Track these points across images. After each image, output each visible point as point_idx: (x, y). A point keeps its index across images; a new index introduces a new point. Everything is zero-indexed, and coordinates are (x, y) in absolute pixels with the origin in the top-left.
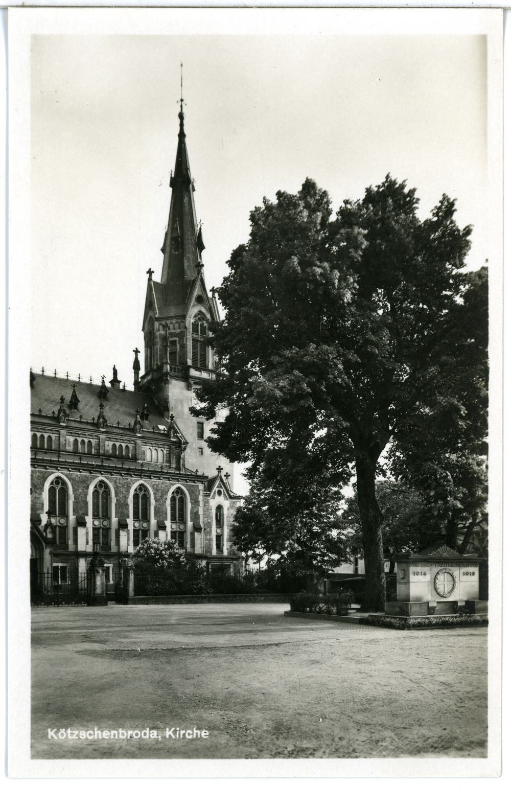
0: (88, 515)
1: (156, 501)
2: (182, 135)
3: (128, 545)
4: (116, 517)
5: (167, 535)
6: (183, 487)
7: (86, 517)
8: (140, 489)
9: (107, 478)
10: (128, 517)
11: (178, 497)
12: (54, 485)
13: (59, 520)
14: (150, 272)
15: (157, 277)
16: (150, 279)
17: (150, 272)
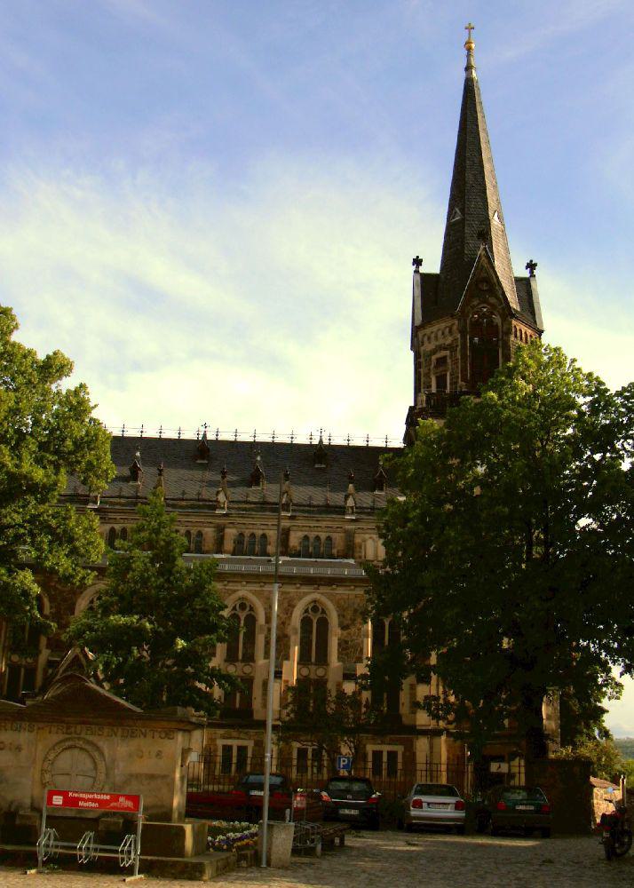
1: (344, 627)
2: (468, 68)
6: (323, 599)
8: (315, 609)
9: (255, 593)
11: (243, 615)
12: (311, 614)
14: (417, 262)
15: (433, 266)
16: (416, 272)
17: (417, 262)
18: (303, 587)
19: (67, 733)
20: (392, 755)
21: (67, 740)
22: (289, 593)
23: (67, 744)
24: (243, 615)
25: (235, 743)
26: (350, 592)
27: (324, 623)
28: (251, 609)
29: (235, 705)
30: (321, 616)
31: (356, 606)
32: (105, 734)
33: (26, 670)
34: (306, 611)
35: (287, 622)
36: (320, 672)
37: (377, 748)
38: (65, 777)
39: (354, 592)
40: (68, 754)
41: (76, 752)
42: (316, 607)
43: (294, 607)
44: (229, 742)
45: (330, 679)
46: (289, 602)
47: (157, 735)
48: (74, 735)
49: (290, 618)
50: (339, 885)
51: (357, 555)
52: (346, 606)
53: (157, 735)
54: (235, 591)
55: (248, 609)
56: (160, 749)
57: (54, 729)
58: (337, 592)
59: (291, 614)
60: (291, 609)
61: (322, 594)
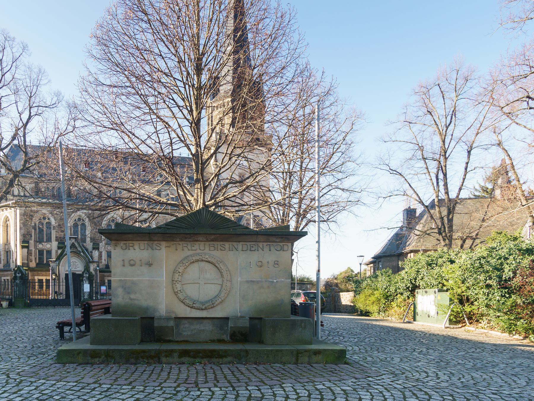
4: (91, 242)
8: (79, 219)
11: (79, 223)
24: (79, 223)
25: (44, 278)
44: (40, 278)
54: (37, 212)
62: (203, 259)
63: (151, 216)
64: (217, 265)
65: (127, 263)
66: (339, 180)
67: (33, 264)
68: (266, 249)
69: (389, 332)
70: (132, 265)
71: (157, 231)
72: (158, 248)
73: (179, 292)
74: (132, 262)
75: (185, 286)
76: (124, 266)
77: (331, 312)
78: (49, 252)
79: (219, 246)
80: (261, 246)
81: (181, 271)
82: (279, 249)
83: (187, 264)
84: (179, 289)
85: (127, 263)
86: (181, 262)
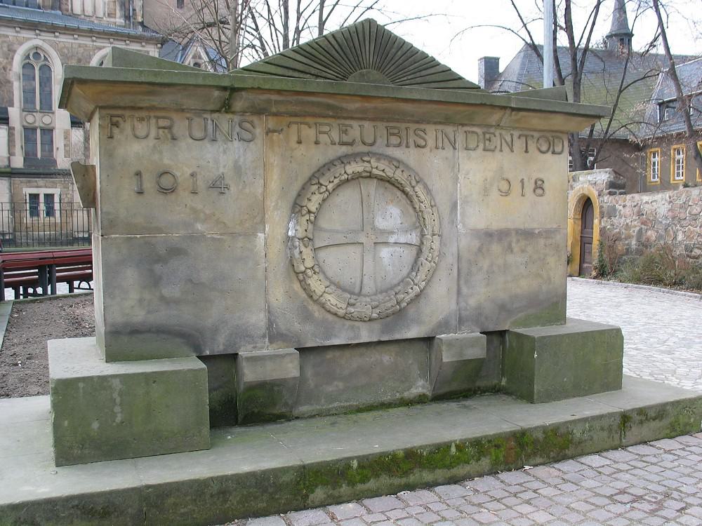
0: (13, 106)
3: (11, 153)
5: (87, 139)
7: (10, 109)
10: (12, 105)
13: (35, 122)
18: (23, 31)
19: (343, 144)
20: (49, 197)
21: (343, 160)
22: (7, 36)
23: (354, 168)
26: (73, 41)
27: (46, 69)
28: (46, 59)
29: (36, 155)
30: (43, 63)
31: (80, 56)
32: (431, 143)
33: (42, 130)
34: (28, 57)
35: (9, 67)
36: (30, 119)
37: (34, 191)
38: (351, 249)
39: (76, 41)
40: (348, 197)
41: (371, 187)
42: (37, 52)
43: (15, 52)
45: (57, 126)
46: (8, 46)
47: (532, 147)
48: (361, 148)
49: (11, 63)
50: (282, 423)
51: (64, 7)
52: (70, 54)
53: (532, 147)
55: (43, 58)
56: (541, 176)
57: (309, 133)
58: (60, 40)
59: (13, 59)
60: (11, 54)
61: (43, 40)
62: (375, 172)
63: (298, 32)
64: (408, 189)
65: (149, 184)
66: (371, 8)
67: (18, 162)
68: (519, 144)
69: (223, 493)
70: (165, 191)
71: (258, 80)
72: (247, 136)
73: (309, 272)
74: (166, 181)
75: (322, 255)
76: (140, 193)
77: (54, 433)
78: (48, 131)
79: (411, 132)
80: (509, 139)
81: (313, 209)
82: (544, 148)
83: (330, 187)
84: (309, 263)
85: (149, 184)
86: (315, 178)
